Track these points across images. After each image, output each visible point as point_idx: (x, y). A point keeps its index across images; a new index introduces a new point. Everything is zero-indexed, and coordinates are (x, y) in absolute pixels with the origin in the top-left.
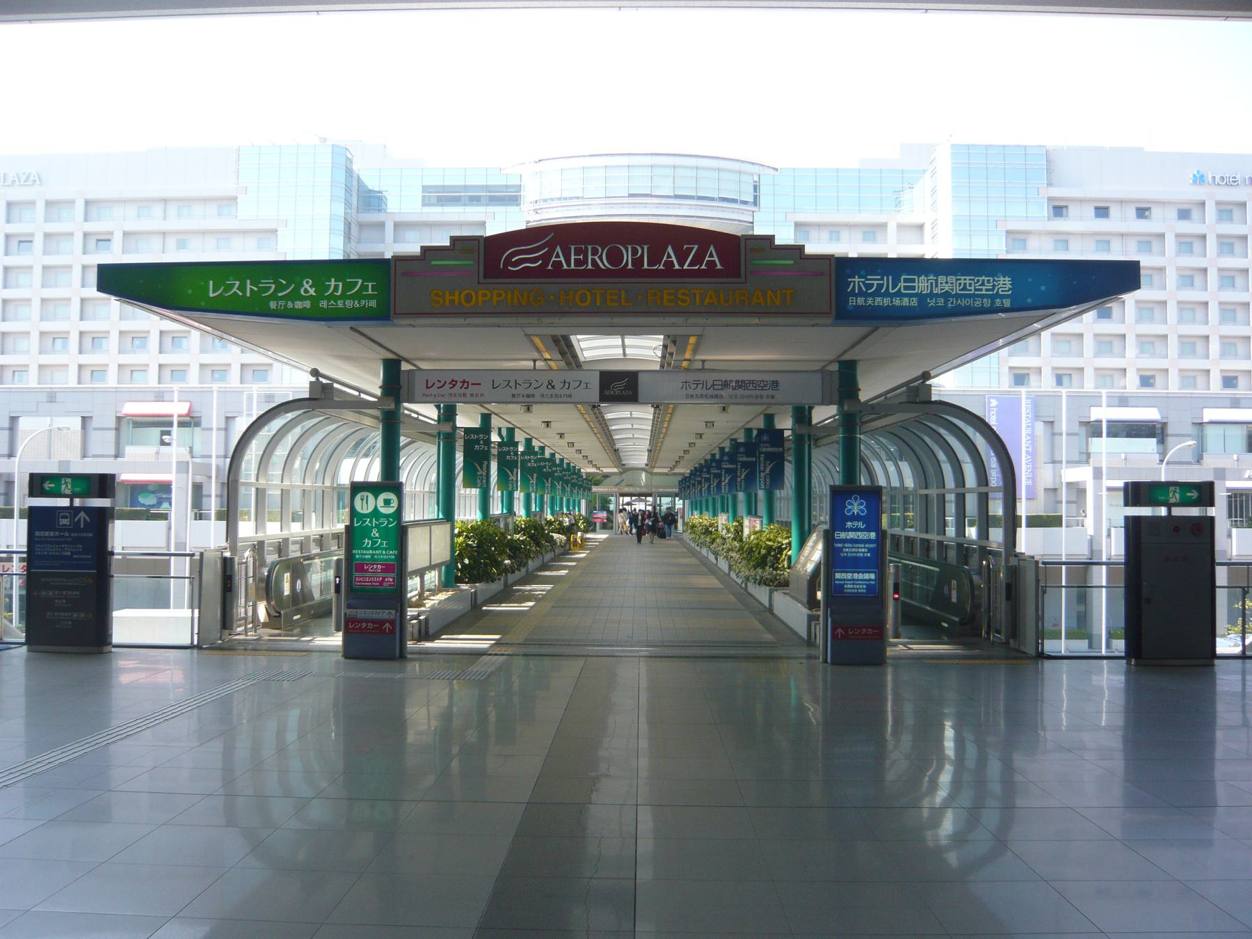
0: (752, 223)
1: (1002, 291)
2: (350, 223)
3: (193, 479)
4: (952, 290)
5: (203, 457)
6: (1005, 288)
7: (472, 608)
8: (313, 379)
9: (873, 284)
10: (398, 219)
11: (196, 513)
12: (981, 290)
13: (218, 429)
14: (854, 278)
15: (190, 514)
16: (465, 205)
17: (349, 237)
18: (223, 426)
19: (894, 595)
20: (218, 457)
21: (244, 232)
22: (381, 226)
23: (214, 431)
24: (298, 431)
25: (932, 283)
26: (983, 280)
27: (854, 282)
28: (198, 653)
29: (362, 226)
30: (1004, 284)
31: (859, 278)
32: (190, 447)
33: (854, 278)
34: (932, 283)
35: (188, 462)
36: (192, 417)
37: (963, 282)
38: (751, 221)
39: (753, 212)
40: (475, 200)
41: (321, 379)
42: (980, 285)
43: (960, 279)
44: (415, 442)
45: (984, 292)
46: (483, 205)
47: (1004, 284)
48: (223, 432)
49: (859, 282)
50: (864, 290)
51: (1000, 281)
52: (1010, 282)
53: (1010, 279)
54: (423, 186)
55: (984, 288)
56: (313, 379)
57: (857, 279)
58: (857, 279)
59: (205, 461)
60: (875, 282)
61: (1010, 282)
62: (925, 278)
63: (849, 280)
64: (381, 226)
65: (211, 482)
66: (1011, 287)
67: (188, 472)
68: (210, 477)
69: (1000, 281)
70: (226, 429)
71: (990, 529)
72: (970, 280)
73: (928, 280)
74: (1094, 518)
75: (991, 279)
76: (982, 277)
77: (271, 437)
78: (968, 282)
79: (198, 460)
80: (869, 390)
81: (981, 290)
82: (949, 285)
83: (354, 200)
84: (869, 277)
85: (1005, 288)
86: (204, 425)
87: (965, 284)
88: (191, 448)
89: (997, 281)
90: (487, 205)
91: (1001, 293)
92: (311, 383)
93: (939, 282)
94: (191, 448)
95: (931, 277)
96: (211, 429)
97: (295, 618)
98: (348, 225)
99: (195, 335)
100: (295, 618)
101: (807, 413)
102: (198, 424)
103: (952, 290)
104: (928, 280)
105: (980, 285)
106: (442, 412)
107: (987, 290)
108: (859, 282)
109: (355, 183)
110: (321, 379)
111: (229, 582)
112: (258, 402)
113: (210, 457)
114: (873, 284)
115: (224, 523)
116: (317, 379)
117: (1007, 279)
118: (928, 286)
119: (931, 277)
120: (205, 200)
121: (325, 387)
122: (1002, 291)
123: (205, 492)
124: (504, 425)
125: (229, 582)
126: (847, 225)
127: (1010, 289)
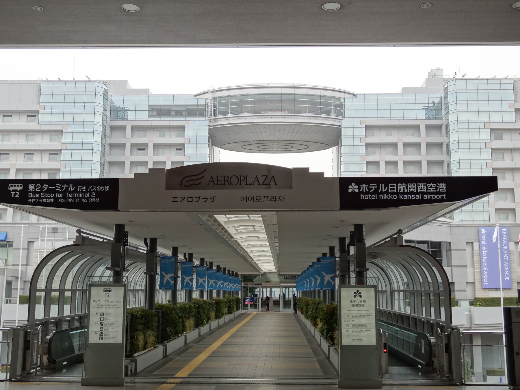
0: (341, 126)
1: (442, 190)
2: (106, 127)
3: (6, 278)
4: (415, 190)
5: (13, 265)
6: (443, 188)
7: (163, 357)
8: (78, 235)
9: (373, 188)
10: (134, 124)
11: (7, 300)
12: (430, 190)
13: (23, 249)
14: (363, 185)
15: (4, 300)
16: (173, 117)
17: (105, 135)
18: (26, 247)
19: (384, 349)
20: (22, 265)
21: (43, 132)
22: (124, 128)
23: (21, 249)
24: (66, 264)
25: (404, 188)
26: (431, 185)
27: (363, 187)
28: (9, 384)
29: (113, 128)
30: (442, 187)
31: (365, 185)
32: (5, 259)
33: (363, 185)
34: (404, 188)
35: (4, 269)
36: (7, 241)
37: (420, 186)
38: (340, 125)
39: (341, 120)
40: (179, 114)
41: (82, 234)
42: (429, 188)
43: (419, 185)
44: (136, 262)
45: (432, 191)
46: (183, 116)
47: (442, 187)
48: (26, 250)
49: (365, 187)
50: (367, 190)
51: (440, 185)
52: (445, 186)
53: (445, 184)
54: (149, 105)
55: (432, 189)
56: (78, 235)
57: (364, 186)
58: (364, 186)
59: (15, 268)
60: (374, 187)
61: (445, 186)
62: (401, 185)
63: (361, 186)
64: (124, 128)
65: (18, 280)
66: (445, 188)
67: (4, 275)
68: (17, 278)
69: (440, 185)
70: (28, 249)
71: (452, 308)
72: (424, 185)
73: (402, 186)
74: (503, 301)
75: (435, 185)
76: (430, 184)
77: (48, 276)
78: (423, 186)
79: (10, 267)
80: (369, 242)
81: (430, 190)
82: (413, 188)
83: (108, 113)
84: (371, 185)
85: (443, 188)
86: (15, 246)
87: (421, 187)
88: (6, 260)
89: (438, 185)
90: (186, 117)
91: (441, 191)
92: (76, 236)
93: (408, 187)
94: (6, 260)
95: (404, 184)
96: (19, 249)
97: (64, 364)
98: (104, 128)
99: (10, 210)
100: (64, 364)
101: (347, 248)
102: (11, 245)
103: (415, 190)
104: (402, 186)
105: (429, 188)
106: (149, 248)
107: (433, 190)
108: (365, 187)
109: (109, 103)
110: (82, 234)
111: (28, 344)
112: (48, 233)
113: (18, 265)
114: (373, 188)
115: (27, 306)
116: (80, 235)
117: (444, 184)
118: (402, 188)
119: (404, 184)
120: (20, 112)
121: (84, 239)
122: (442, 190)
123: (13, 286)
124: (188, 251)
125: (28, 344)
126: (396, 127)
127: (445, 189)
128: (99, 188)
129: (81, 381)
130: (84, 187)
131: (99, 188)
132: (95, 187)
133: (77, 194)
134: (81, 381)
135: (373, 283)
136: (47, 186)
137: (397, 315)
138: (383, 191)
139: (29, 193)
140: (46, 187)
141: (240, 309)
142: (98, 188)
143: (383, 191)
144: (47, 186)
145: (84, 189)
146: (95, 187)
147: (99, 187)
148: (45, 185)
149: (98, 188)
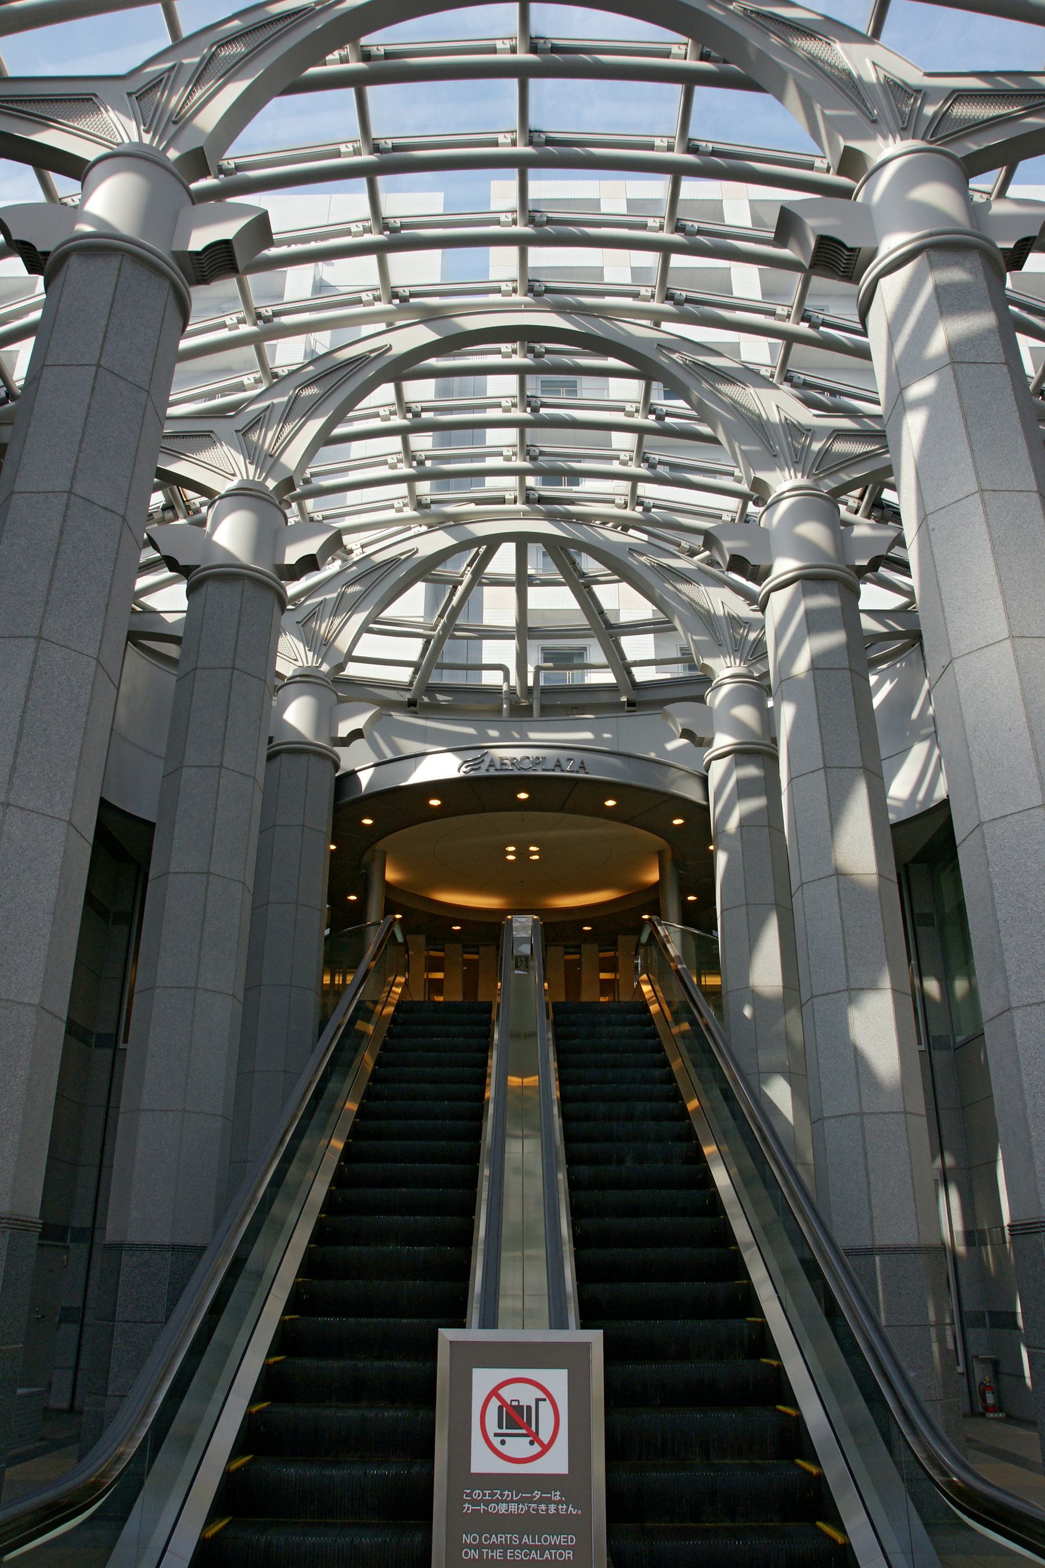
128: (495, 1507)
129: (643, 383)
130: (543, 1505)
131: (495, 1507)
132: (499, 1492)
133: (509, 1554)
134: (643, 383)
135: (820, 769)
136: (540, 1493)
137: (700, 569)
138: (514, 1499)
139: (509, 1551)
140: (538, 1494)
141: (763, 506)
142: (491, 1507)
143: (514, 1499)
144: (540, 1493)
145: (542, 1511)
146: (499, 1492)
147: (477, 1491)
148: (536, 1492)
149: (491, 1507)
